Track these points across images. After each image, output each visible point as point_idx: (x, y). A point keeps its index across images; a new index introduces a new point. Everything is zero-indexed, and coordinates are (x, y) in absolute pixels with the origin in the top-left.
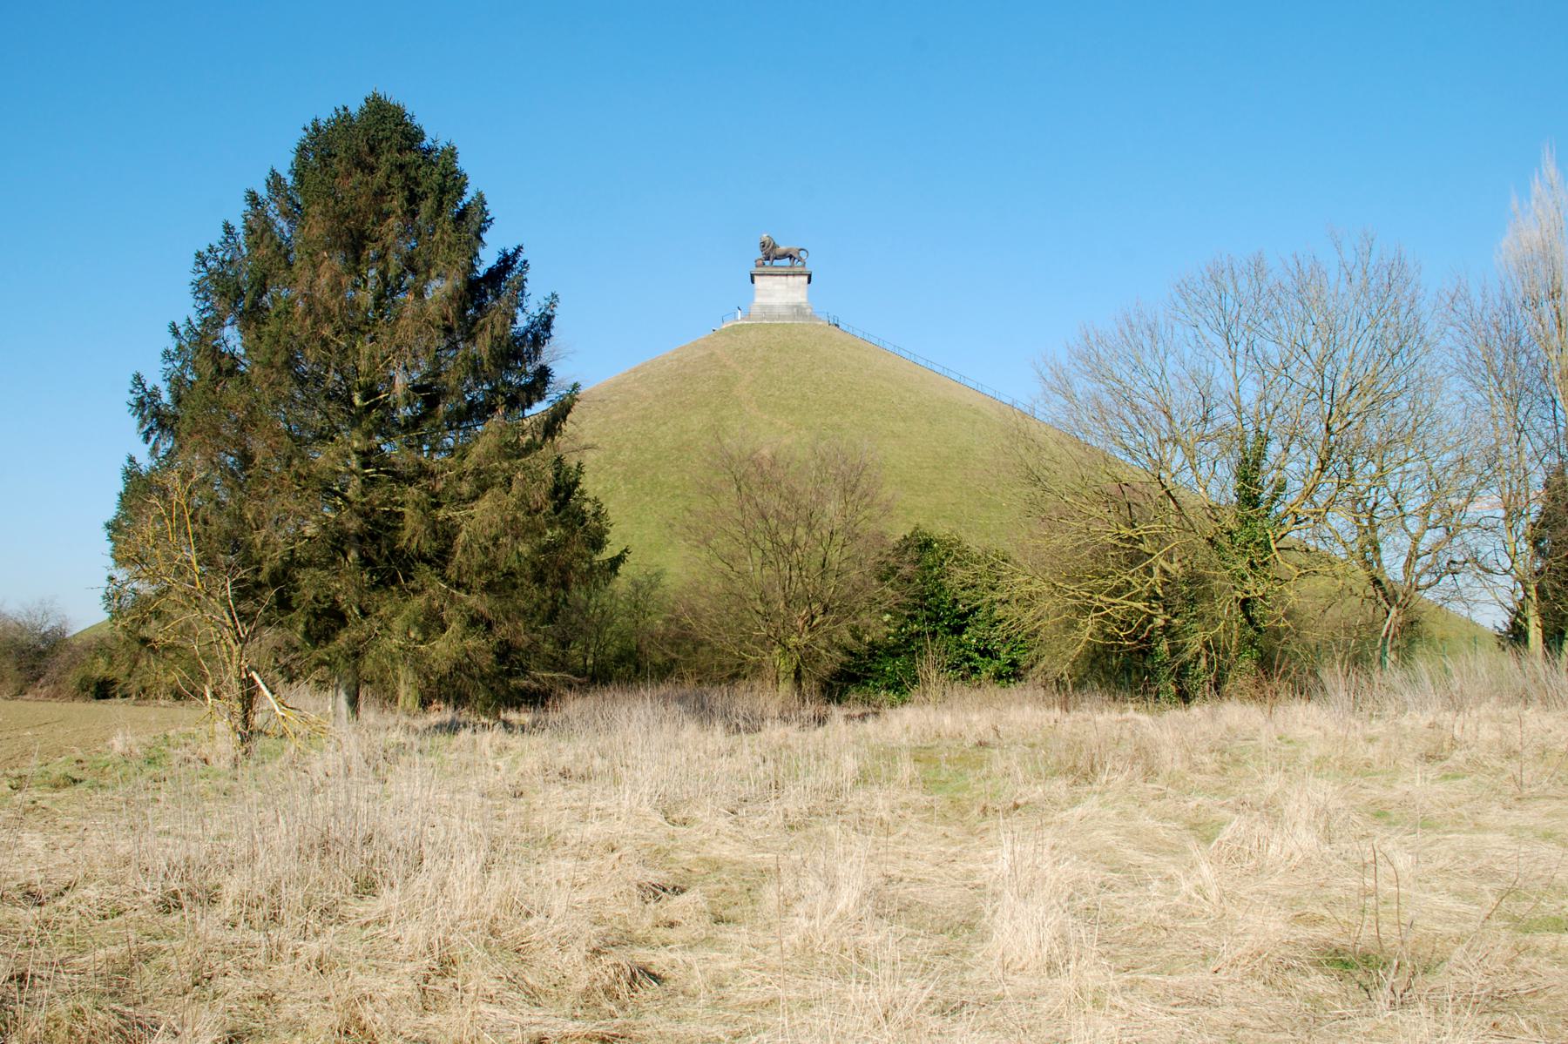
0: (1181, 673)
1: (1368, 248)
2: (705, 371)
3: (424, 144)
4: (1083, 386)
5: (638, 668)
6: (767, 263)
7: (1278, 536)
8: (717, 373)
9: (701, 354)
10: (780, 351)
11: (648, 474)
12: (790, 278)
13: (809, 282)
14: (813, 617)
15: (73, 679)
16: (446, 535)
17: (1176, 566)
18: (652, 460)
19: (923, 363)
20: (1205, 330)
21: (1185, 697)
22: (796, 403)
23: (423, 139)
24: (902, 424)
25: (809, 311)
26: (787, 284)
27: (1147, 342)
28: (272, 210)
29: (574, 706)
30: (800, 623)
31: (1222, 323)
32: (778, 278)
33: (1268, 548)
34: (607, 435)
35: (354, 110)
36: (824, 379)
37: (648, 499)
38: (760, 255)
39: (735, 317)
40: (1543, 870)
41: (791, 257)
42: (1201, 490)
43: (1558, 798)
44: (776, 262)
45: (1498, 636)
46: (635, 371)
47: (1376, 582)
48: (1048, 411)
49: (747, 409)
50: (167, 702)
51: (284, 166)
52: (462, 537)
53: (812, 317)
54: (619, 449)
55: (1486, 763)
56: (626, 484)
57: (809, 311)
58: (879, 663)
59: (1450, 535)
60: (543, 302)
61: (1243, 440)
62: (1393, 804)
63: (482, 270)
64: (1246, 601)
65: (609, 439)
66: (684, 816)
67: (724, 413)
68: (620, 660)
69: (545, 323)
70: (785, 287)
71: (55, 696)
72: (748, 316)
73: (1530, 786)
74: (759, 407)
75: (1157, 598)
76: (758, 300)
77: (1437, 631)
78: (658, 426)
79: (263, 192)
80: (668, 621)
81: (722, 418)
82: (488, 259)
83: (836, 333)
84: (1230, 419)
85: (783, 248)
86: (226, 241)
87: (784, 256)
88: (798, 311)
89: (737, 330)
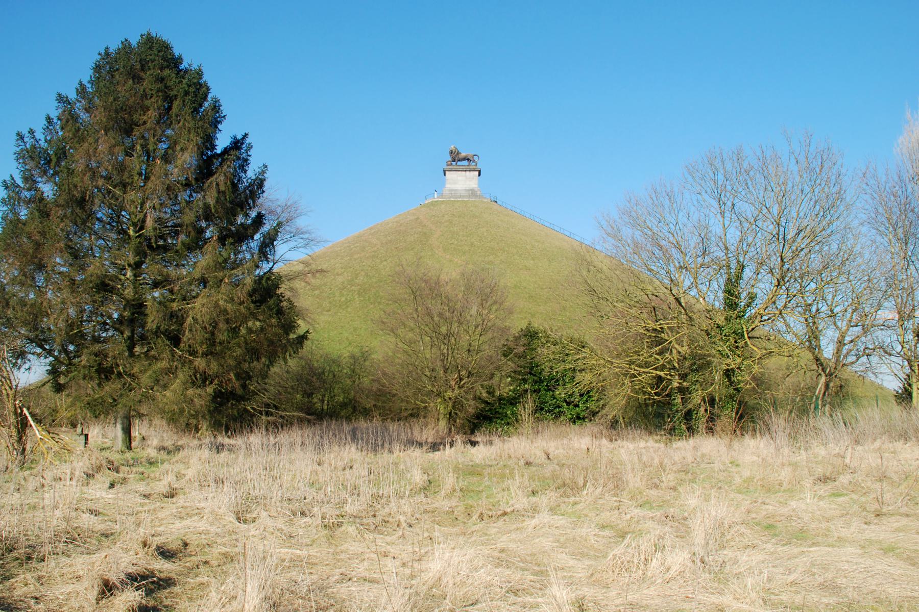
0: (688, 415)
1: (808, 141)
2: (412, 228)
3: (182, 67)
4: (627, 232)
5: (354, 409)
6: (454, 163)
7: (750, 329)
9: (411, 218)
11: (373, 291)
12: (468, 173)
13: (479, 175)
14: (461, 379)
16: (177, 318)
17: (686, 348)
18: (376, 283)
19: (547, 225)
20: (706, 197)
21: (691, 430)
22: (467, 248)
23: (181, 63)
24: (532, 262)
25: (479, 193)
26: (466, 176)
27: (666, 203)
28: (79, 108)
29: (295, 435)
30: (453, 383)
31: (716, 191)
32: (460, 172)
33: (743, 336)
35: (134, 42)
36: (485, 234)
37: (372, 306)
38: (450, 159)
39: (434, 196)
40: (877, 585)
41: (468, 160)
42: (701, 299)
43: (907, 516)
44: (459, 163)
45: (896, 396)
46: (371, 229)
47: (817, 360)
48: (602, 245)
49: (437, 252)
50: (67, 429)
51: (86, 75)
52: (189, 320)
54: (357, 276)
55: (863, 485)
56: (359, 297)
57: (479, 193)
58: (504, 408)
59: (865, 331)
60: (257, 170)
61: (729, 267)
62: (782, 518)
63: (220, 148)
64: (728, 370)
65: (351, 269)
66: (254, 516)
67: (423, 254)
68: (344, 405)
69: (259, 184)
72: (441, 195)
73: (889, 505)
74: (444, 251)
75: (674, 368)
76: (448, 186)
77: (859, 392)
78: (382, 262)
79: (72, 96)
82: (222, 142)
83: (495, 206)
84: (721, 254)
85: (463, 154)
86: (48, 127)
87: (464, 159)
88: (472, 192)
89: (433, 204)
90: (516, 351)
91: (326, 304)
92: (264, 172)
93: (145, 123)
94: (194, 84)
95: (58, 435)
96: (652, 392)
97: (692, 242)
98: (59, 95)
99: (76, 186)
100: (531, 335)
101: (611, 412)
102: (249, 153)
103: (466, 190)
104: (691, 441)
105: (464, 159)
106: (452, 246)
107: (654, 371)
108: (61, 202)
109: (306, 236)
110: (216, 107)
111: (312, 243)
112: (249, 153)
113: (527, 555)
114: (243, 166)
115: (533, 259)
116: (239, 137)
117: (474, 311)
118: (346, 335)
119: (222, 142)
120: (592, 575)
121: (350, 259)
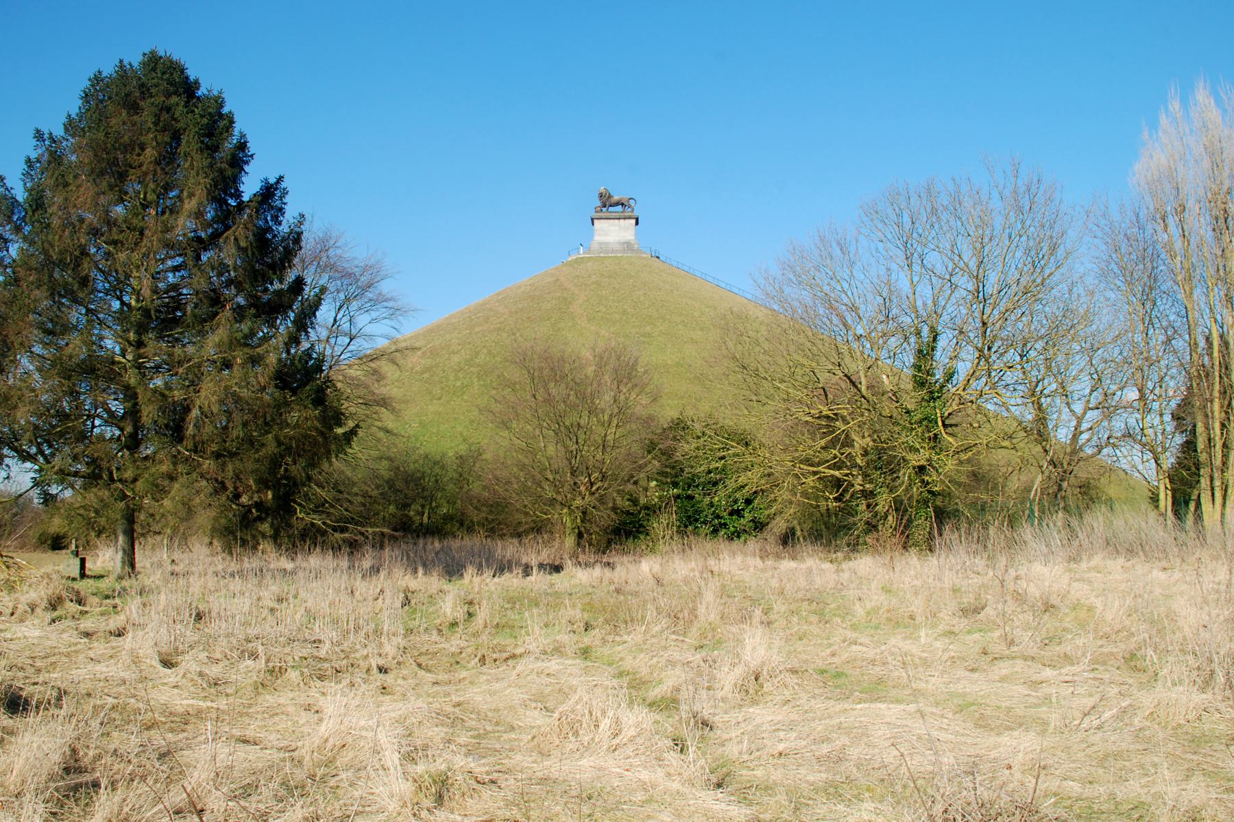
3: (199, 93)
6: (604, 209)
7: (946, 414)
8: (559, 294)
10: (610, 277)
12: (622, 221)
13: (637, 223)
14: (592, 484)
15: (34, 534)
18: (501, 362)
19: (723, 285)
22: (617, 316)
24: (700, 333)
25: (636, 246)
34: (470, 343)
36: (642, 298)
38: (599, 204)
41: (622, 204)
46: (498, 294)
51: (74, 106)
53: (638, 251)
54: (477, 354)
56: (479, 380)
57: (636, 246)
68: (448, 518)
69: (297, 238)
70: (617, 228)
71: (21, 548)
72: (589, 250)
74: (589, 320)
75: (855, 465)
76: (597, 238)
77: (1112, 491)
80: (485, 488)
81: (559, 329)
82: (250, 186)
85: (616, 198)
87: (617, 204)
88: (628, 246)
89: (579, 261)
90: (660, 446)
91: (437, 391)
92: (301, 223)
93: (141, 165)
94: (210, 114)
95: (12, 558)
96: (831, 497)
97: (870, 307)
98: (38, 131)
99: (52, 246)
100: (679, 427)
101: (779, 526)
102: (285, 201)
103: (620, 243)
104: (933, 561)
105: (617, 204)
106: (600, 314)
107: (826, 471)
108: (33, 263)
109: (390, 304)
110: (242, 146)
111: (398, 313)
112: (285, 201)
113: (490, 710)
114: (277, 217)
115: (702, 329)
116: (272, 181)
117: (608, 397)
118: (460, 429)
119: (250, 186)
120: (534, 737)
121: (470, 333)
